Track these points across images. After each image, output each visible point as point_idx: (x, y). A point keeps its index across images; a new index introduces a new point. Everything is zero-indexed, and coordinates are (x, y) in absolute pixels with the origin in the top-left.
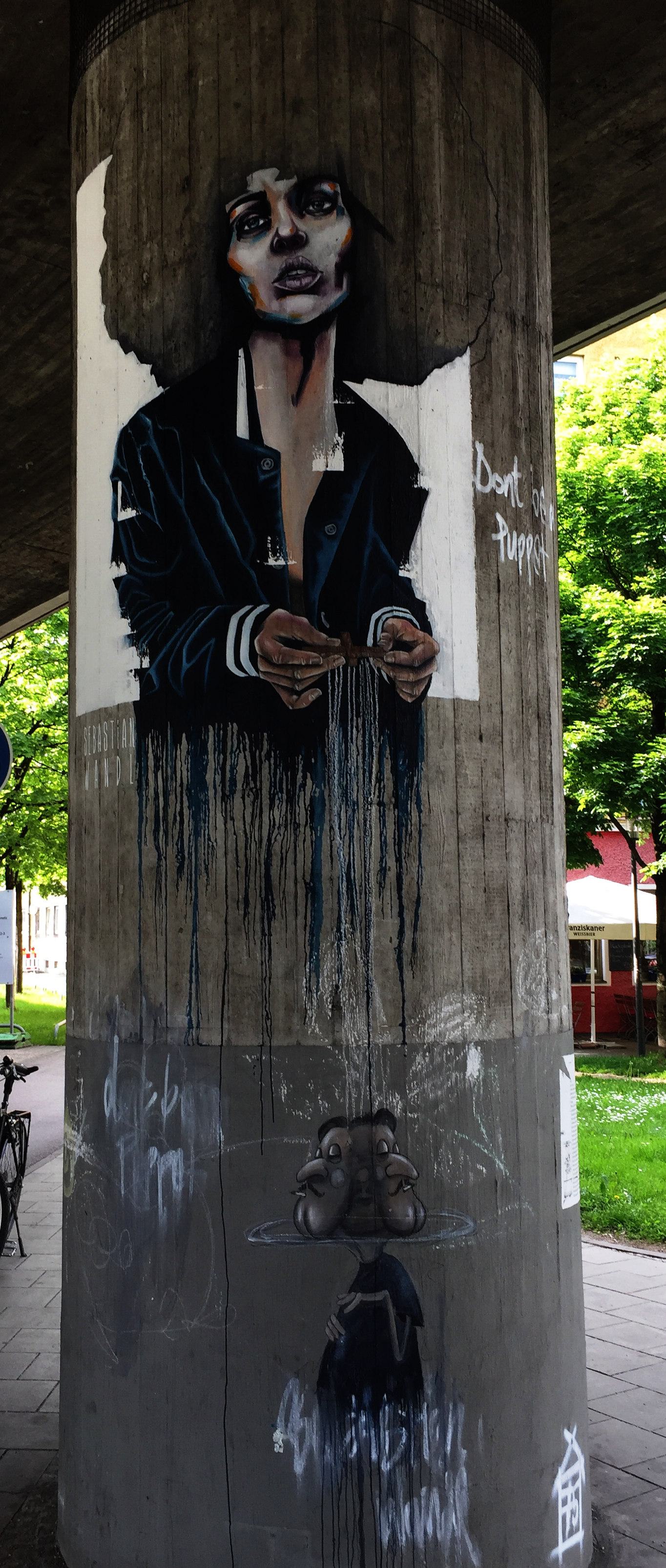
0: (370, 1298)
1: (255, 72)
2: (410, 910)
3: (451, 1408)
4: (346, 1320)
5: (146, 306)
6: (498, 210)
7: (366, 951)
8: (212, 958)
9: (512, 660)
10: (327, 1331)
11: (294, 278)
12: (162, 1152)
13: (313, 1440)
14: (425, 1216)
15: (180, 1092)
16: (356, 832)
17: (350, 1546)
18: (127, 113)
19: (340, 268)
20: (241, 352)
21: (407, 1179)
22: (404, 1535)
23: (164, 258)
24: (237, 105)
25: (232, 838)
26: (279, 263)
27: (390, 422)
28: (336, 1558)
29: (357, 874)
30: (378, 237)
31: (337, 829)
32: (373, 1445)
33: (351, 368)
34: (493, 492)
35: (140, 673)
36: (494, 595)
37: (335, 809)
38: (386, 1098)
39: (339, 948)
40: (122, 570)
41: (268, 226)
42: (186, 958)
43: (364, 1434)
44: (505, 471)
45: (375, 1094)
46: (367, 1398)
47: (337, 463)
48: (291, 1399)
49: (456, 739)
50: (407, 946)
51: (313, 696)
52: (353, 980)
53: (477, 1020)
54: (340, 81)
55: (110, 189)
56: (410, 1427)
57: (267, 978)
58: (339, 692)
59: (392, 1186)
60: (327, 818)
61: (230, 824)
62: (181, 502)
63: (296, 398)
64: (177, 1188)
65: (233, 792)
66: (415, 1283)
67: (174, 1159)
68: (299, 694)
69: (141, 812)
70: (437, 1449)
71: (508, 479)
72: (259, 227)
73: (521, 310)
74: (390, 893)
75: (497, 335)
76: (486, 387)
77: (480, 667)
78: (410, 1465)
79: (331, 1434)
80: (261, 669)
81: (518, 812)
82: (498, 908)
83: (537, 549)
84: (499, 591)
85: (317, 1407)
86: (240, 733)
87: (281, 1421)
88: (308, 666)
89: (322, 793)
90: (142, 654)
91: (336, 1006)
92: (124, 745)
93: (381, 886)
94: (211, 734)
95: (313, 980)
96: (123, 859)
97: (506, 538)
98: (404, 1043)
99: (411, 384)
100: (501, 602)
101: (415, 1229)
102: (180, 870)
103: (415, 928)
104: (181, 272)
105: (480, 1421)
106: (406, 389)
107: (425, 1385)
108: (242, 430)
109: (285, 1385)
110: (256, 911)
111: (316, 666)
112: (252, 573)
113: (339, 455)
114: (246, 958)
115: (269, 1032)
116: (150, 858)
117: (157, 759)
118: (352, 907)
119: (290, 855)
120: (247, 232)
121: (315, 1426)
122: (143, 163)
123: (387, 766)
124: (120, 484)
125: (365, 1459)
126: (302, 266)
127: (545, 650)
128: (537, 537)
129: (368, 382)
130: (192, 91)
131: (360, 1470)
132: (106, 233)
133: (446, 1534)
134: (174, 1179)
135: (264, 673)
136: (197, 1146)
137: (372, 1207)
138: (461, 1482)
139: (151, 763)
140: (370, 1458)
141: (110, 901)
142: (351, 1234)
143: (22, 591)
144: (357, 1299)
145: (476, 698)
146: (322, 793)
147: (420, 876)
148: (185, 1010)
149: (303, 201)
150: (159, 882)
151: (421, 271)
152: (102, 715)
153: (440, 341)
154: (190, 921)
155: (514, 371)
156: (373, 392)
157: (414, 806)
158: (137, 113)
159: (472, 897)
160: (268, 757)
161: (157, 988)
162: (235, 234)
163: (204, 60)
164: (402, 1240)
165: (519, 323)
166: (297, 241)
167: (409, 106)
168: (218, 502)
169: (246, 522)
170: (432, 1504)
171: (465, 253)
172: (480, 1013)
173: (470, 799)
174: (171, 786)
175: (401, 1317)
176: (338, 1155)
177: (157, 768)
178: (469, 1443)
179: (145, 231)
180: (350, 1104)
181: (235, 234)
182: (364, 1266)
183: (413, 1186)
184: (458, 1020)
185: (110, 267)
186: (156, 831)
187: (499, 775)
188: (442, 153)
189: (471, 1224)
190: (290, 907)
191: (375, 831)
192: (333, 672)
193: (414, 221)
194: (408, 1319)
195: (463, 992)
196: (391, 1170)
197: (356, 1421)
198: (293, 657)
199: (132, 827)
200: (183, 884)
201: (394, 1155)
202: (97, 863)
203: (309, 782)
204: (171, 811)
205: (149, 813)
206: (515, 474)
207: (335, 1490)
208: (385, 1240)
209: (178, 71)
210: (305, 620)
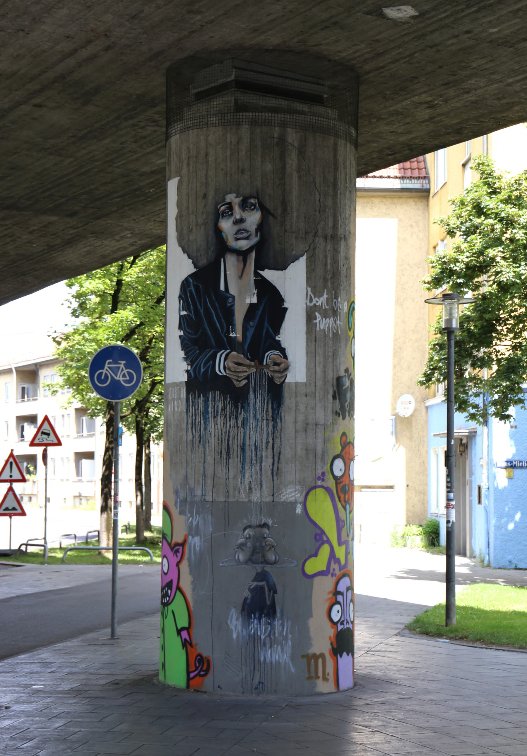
0: (260, 584)
1: (228, 158)
2: (277, 457)
4: (251, 591)
5: (191, 238)
6: (320, 198)
7: (261, 470)
8: (210, 472)
9: (321, 366)
11: (241, 234)
12: (193, 537)
13: (240, 628)
16: (258, 429)
18: (185, 163)
19: (257, 230)
20: (222, 260)
21: (273, 546)
23: (197, 222)
24: (222, 169)
25: (217, 431)
26: (236, 228)
27: (274, 284)
29: (258, 444)
30: (271, 218)
31: (251, 428)
33: (260, 266)
34: (315, 305)
35: (187, 371)
36: (314, 343)
37: (251, 421)
39: (251, 469)
40: (182, 333)
41: (232, 215)
42: (201, 472)
44: (320, 296)
47: (254, 300)
48: (232, 615)
49: (296, 396)
50: (275, 468)
51: (244, 382)
52: (256, 479)
53: (301, 495)
54: (258, 161)
55: (179, 189)
57: (227, 479)
58: (253, 381)
60: (248, 424)
61: (216, 426)
62: (202, 311)
63: (241, 277)
64: (198, 549)
65: (217, 415)
66: (275, 581)
67: (197, 539)
68: (240, 381)
69: (187, 421)
71: (322, 299)
72: (229, 215)
73: (330, 232)
74: (270, 450)
75: (318, 245)
76: (313, 267)
77: (307, 370)
80: (227, 372)
81: (322, 421)
82: (311, 456)
83: (335, 323)
84: (316, 341)
86: (220, 395)
88: (243, 372)
89: (247, 416)
90: (188, 365)
91: (250, 488)
92: (182, 397)
93: (266, 448)
94: (210, 394)
95: (243, 479)
96: (181, 437)
97: (320, 321)
98: (273, 501)
99: (282, 270)
100: (317, 346)
101: (275, 563)
102: (200, 441)
103: (278, 462)
104: (202, 228)
105: (297, 627)
106: (280, 272)
108: (222, 288)
110: (224, 455)
111: (246, 372)
112: (225, 338)
113: (255, 297)
114: (221, 472)
115: (228, 497)
116: (190, 437)
117: (193, 402)
118: (256, 455)
119: (236, 437)
120: (225, 216)
122: (190, 186)
123: (270, 406)
124: (181, 301)
126: (243, 230)
127: (338, 360)
128: (336, 318)
129: (266, 270)
130: (207, 162)
131: (254, 638)
132: (178, 207)
135: (229, 374)
139: (191, 404)
141: (177, 452)
142: (253, 563)
143: (149, 240)
145: (305, 381)
146: (247, 416)
147: (281, 445)
148: (201, 489)
149: (244, 205)
150: (193, 446)
151: (287, 228)
152: (175, 385)
153: (294, 252)
154: (203, 459)
155: (326, 257)
156: (268, 274)
157: (279, 420)
158: (188, 164)
159: (300, 451)
160: (229, 403)
161: (191, 482)
162: (221, 216)
163: (211, 151)
164: (270, 566)
165: (329, 238)
166: (241, 221)
167: (284, 168)
168: (214, 313)
169: (223, 320)
171: (305, 217)
172: (302, 492)
173: (301, 418)
174: (197, 412)
175: (269, 591)
176: (250, 538)
177: (193, 405)
179: (191, 212)
181: (221, 216)
182: (257, 574)
184: (293, 494)
185: (179, 218)
186: (192, 428)
187: (314, 408)
188: (297, 182)
189: (295, 562)
190: (235, 455)
191: (265, 429)
192: (251, 374)
193: (285, 210)
194: (272, 591)
195: (296, 485)
196: (267, 543)
197: (253, 622)
198: (238, 369)
199: (184, 426)
200: (201, 446)
202: (173, 438)
203: (243, 412)
204: (197, 421)
205: (190, 421)
206: (325, 296)
209: (203, 153)
210: (242, 356)
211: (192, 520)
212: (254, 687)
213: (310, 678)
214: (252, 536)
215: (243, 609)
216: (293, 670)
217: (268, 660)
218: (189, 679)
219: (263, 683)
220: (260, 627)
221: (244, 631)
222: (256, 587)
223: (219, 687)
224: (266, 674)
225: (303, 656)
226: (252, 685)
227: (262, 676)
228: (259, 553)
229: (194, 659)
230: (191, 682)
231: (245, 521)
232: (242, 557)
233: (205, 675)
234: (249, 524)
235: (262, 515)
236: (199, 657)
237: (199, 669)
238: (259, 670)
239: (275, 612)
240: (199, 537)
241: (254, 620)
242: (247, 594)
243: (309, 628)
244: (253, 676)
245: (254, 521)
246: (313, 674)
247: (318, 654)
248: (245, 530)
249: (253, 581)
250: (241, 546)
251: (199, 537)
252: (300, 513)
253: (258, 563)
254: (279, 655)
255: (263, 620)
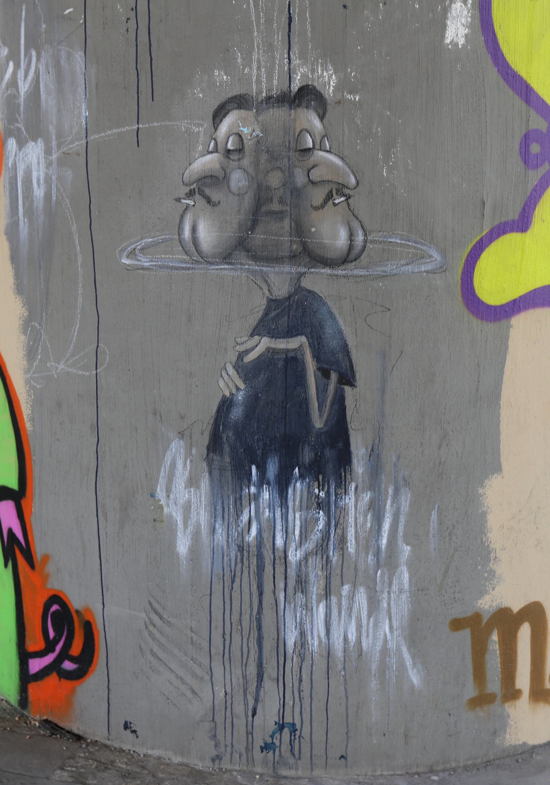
0: (282, 344)
3: (391, 491)
4: (248, 372)
10: (222, 384)
12: (21, 144)
13: (202, 516)
14: (365, 241)
15: (38, 59)
17: (245, 645)
21: (341, 189)
22: (316, 638)
28: (227, 655)
32: (279, 527)
38: (313, 71)
43: (267, 514)
45: (296, 62)
46: (272, 469)
48: (173, 465)
56: (329, 510)
59: (318, 195)
64: (39, 192)
67: (34, 152)
70: (368, 541)
78: (328, 557)
79: (223, 508)
85: (207, 475)
87: (162, 490)
101: (349, 257)
107: (355, 461)
109: (166, 448)
121: (203, 499)
125: (268, 545)
131: (260, 557)
133: (374, 644)
134: (35, 181)
136: (59, 136)
137: (287, 222)
138: (401, 583)
140: (274, 544)
142: (255, 258)
144: (261, 344)
164: (328, 271)
170: (356, 607)
175: (325, 373)
176: (240, 150)
178: (415, 537)
180: (259, 76)
182: (273, 304)
183: (348, 197)
189: (436, 256)
194: (334, 376)
196: (315, 175)
197: (257, 497)
201: (321, 153)
207: (227, 578)
208: (303, 270)
211: (15, 73)
212: (259, 743)
213: (482, 700)
214: (249, 144)
215: (215, 444)
216: (415, 678)
217: (314, 643)
218: (26, 679)
219: (293, 730)
220: (285, 517)
221: (220, 530)
222: (268, 360)
223: (126, 726)
224: (306, 694)
225: (457, 624)
226: (249, 733)
227: (289, 701)
228: (279, 215)
229: (40, 611)
230: (32, 688)
231: (220, 76)
232: (208, 234)
233: (79, 675)
234: (236, 92)
235: (295, 49)
236: (55, 607)
237: (58, 648)
238: (281, 679)
239: (344, 459)
240: (40, 143)
241: (260, 486)
242: (230, 384)
243: (484, 514)
244: (257, 700)
245: (261, 76)
246: (494, 685)
247: (516, 608)
248: (219, 115)
249: (256, 332)
250: (205, 187)
251: (40, 143)
252: (461, 41)
253: (277, 260)
254: (361, 626)
255: (297, 489)
